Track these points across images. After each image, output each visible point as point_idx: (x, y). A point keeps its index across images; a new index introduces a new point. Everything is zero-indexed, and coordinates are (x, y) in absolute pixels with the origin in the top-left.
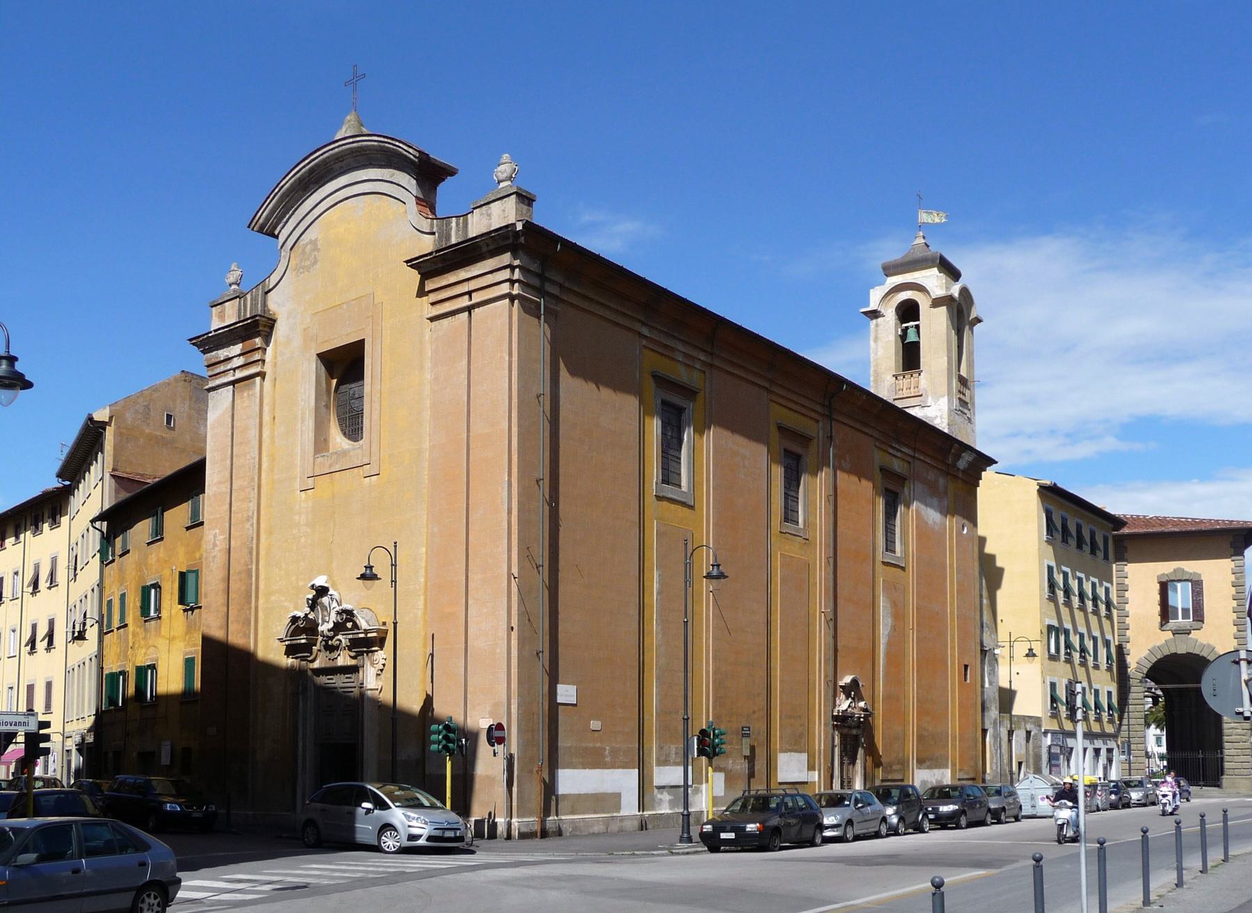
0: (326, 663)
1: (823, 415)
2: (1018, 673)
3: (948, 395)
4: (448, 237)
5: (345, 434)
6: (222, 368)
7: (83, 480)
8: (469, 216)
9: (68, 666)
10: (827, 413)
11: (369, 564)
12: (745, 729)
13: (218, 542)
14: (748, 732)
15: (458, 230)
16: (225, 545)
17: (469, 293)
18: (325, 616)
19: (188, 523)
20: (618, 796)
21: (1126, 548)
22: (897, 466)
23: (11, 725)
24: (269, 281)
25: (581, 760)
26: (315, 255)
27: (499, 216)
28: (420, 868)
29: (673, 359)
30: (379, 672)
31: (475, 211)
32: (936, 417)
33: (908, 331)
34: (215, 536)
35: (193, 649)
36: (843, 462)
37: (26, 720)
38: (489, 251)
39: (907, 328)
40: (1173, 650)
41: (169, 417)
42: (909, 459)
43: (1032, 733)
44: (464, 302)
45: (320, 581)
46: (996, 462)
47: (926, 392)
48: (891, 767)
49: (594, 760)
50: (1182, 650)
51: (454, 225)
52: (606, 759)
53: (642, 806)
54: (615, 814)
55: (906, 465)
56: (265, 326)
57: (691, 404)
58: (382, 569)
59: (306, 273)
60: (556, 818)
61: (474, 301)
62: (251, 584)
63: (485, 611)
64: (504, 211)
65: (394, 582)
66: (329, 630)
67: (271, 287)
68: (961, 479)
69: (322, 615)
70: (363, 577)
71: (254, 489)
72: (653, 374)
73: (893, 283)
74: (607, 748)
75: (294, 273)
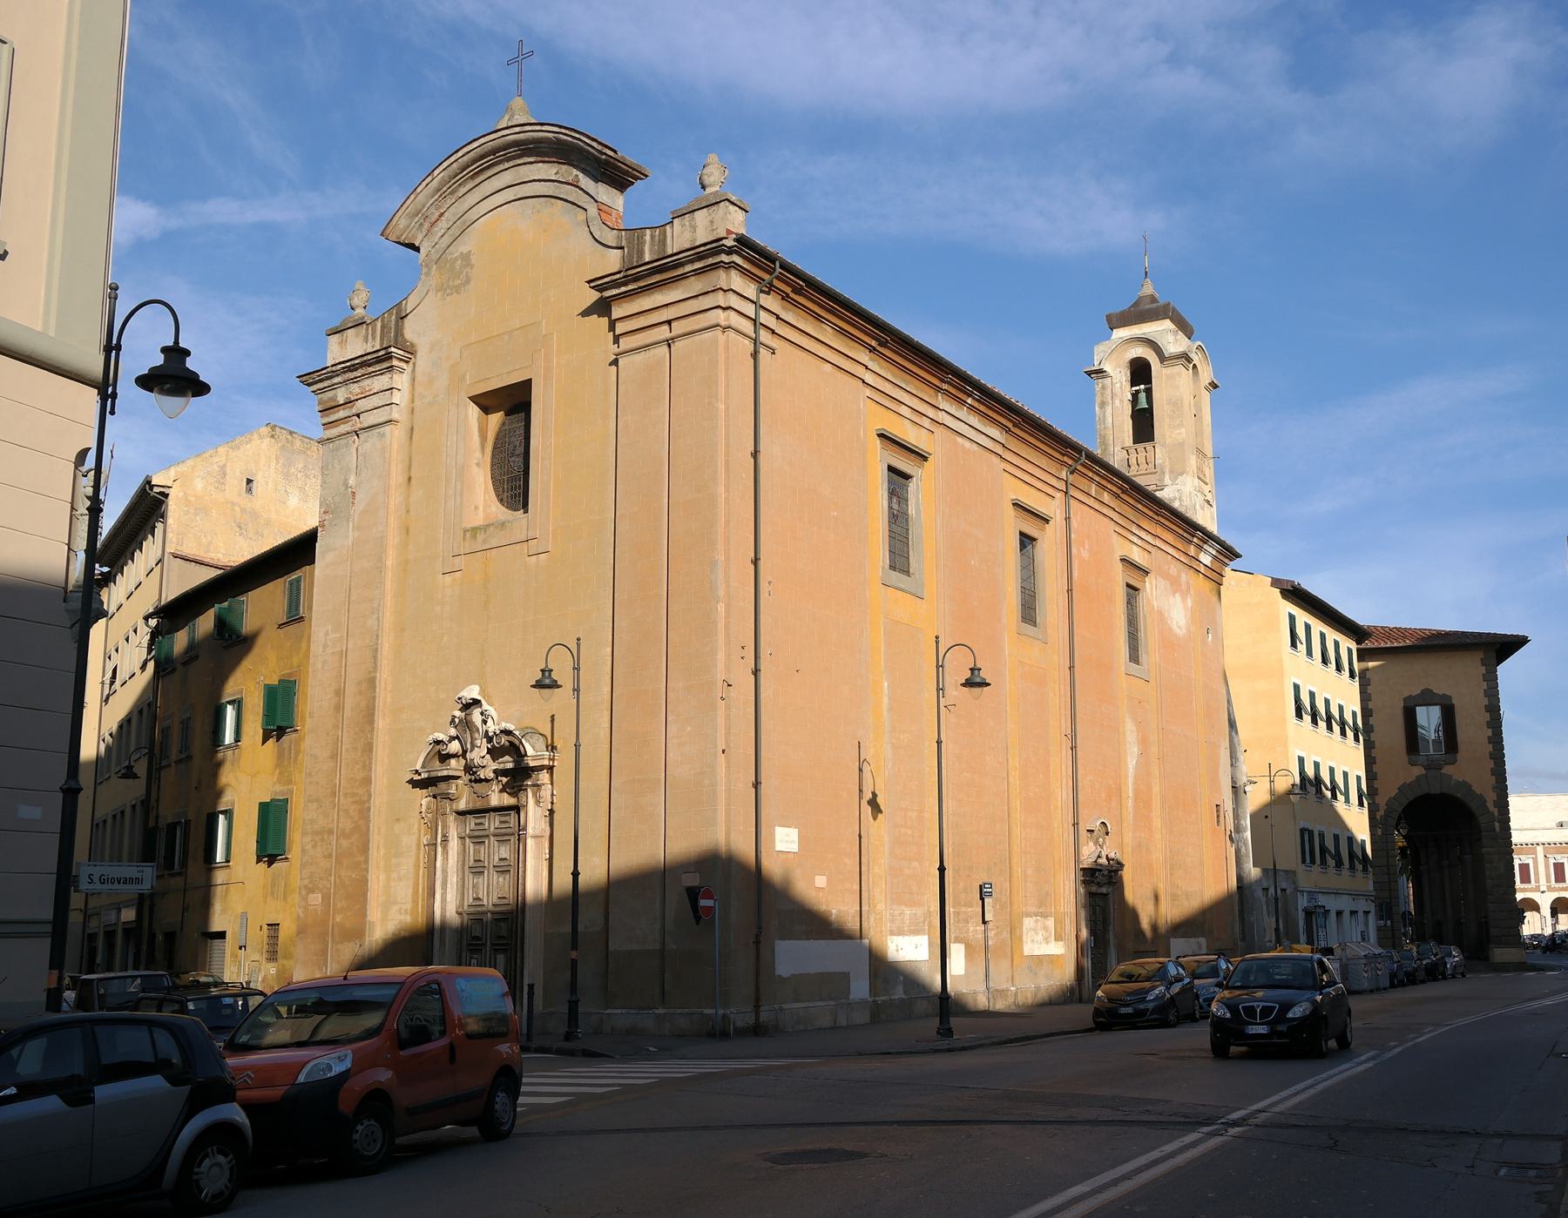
0: (475, 802)
4: (641, 253)
5: (501, 501)
6: (342, 414)
7: (130, 562)
8: (668, 227)
9: (96, 817)
11: (547, 666)
12: (986, 886)
13: (329, 643)
14: (990, 890)
15: (652, 244)
17: (669, 322)
19: (283, 619)
20: (845, 977)
23: (119, 883)
24: (406, 304)
27: (706, 228)
31: (675, 220)
32: (1176, 498)
34: (327, 634)
35: (286, 787)
37: (139, 875)
40: (1426, 791)
41: (249, 481)
44: (664, 333)
45: (473, 692)
51: (648, 238)
53: (873, 990)
58: (563, 674)
59: (455, 294)
60: (877, 999)
61: (674, 334)
64: (712, 222)
65: (577, 690)
67: (408, 312)
70: (539, 685)
73: (486, 488)
75: (439, 294)
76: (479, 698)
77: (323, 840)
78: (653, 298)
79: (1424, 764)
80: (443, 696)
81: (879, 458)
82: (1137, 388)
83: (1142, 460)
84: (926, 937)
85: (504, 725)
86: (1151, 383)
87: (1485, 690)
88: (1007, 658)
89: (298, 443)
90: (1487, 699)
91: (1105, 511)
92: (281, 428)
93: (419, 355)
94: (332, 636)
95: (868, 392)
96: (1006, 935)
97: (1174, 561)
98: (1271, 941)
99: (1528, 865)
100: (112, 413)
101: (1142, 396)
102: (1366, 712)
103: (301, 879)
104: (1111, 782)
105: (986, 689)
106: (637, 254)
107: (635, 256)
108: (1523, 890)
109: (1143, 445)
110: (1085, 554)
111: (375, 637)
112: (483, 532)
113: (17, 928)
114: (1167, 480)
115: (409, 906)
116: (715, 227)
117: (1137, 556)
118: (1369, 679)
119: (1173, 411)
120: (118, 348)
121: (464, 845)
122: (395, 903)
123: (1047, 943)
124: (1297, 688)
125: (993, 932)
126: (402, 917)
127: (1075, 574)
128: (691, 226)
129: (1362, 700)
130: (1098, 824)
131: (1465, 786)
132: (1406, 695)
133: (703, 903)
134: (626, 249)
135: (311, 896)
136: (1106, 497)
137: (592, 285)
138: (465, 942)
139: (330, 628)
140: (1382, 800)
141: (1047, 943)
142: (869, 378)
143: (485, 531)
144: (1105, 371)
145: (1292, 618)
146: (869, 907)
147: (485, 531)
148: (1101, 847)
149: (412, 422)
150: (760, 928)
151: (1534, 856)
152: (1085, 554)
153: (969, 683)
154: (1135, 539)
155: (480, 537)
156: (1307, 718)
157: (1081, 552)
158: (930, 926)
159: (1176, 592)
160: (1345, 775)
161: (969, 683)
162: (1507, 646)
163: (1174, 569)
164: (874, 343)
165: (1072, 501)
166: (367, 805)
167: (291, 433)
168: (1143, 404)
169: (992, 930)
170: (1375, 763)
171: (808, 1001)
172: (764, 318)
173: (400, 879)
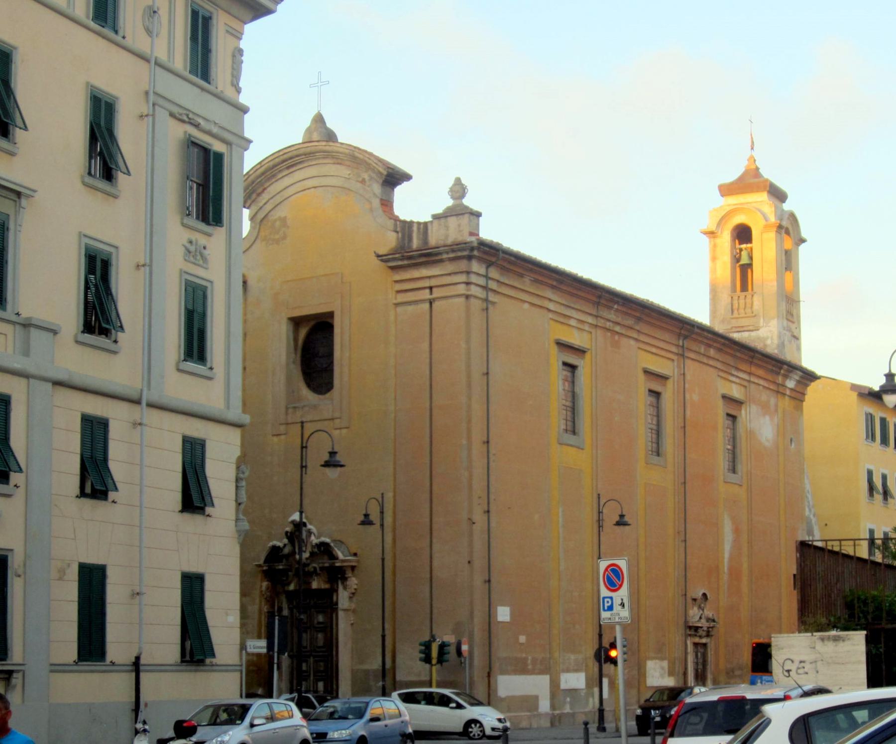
1: (677, 354)
2: (826, 525)
17: (431, 288)
20: (536, 698)
22: (736, 392)
29: (569, 325)
30: (351, 595)
42: (746, 383)
44: (426, 294)
48: (733, 672)
49: (521, 668)
53: (553, 707)
55: (743, 389)
57: (582, 362)
58: (375, 516)
70: (363, 523)
81: (556, 358)
85: (323, 539)
91: (711, 362)
95: (551, 315)
100: (306, 473)
101: (744, 254)
105: (627, 527)
110: (695, 397)
113: (163, 668)
120: (306, 447)
124: (870, 473)
127: (688, 413)
130: (700, 594)
136: (712, 352)
137: (380, 258)
142: (551, 306)
148: (703, 610)
150: (490, 668)
152: (695, 397)
153: (618, 524)
156: (879, 497)
157: (693, 397)
158: (587, 666)
161: (618, 524)
163: (765, 396)
164: (555, 283)
165: (688, 362)
168: (745, 260)
172: (493, 285)
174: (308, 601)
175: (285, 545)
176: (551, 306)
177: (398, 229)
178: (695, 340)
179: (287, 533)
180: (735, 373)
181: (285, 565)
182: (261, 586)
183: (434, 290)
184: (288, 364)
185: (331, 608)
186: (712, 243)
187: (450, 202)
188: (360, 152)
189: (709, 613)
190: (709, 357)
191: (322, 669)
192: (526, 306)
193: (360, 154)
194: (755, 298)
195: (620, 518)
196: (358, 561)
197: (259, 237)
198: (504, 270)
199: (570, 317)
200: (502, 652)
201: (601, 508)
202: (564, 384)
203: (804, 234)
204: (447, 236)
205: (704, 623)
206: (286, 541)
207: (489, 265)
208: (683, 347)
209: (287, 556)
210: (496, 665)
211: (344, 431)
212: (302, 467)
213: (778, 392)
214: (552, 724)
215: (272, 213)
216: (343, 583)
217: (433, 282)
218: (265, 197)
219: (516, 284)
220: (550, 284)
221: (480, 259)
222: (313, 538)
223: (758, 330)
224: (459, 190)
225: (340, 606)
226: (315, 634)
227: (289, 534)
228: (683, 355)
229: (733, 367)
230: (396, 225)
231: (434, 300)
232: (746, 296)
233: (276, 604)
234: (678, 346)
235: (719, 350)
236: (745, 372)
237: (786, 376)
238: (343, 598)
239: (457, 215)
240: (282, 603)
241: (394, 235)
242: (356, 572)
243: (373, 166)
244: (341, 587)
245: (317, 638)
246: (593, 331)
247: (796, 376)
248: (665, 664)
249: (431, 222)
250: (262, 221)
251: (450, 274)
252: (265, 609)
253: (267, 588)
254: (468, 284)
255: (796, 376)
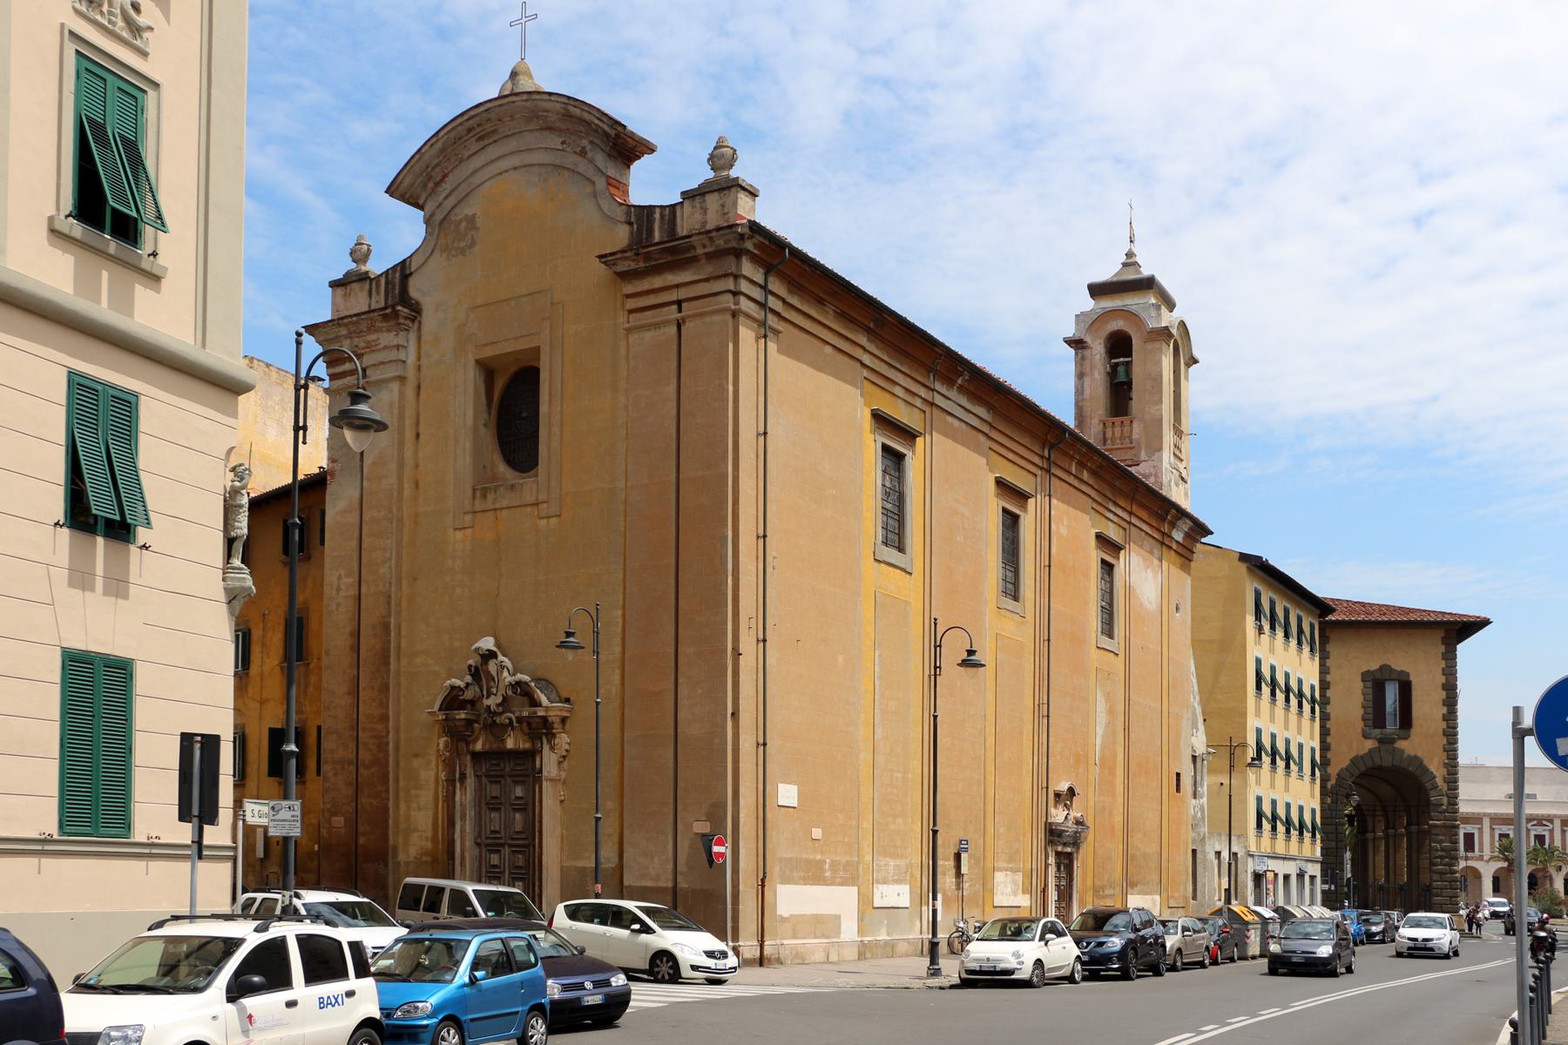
1: (1041, 468)
3: (1072, 433)
4: (650, 231)
10: (1045, 466)
13: (343, 587)
16: (353, 592)
17: (679, 303)
18: (492, 687)
20: (837, 919)
21: (1328, 637)
24: (410, 262)
25: (802, 874)
26: (472, 236)
27: (717, 212)
28: (659, 1002)
30: (561, 759)
33: (1118, 368)
34: (339, 578)
36: (1060, 526)
38: (706, 254)
39: (1117, 365)
42: (1126, 525)
43: (1239, 856)
45: (488, 643)
46: (1212, 533)
47: (1139, 444)
49: (814, 875)
50: (1387, 761)
52: (827, 874)
54: (834, 940)
55: (1121, 531)
56: (406, 318)
62: (389, 642)
63: (700, 691)
64: (723, 206)
66: (498, 705)
68: (1175, 551)
69: (487, 685)
71: (392, 522)
72: (874, 412)
74: (828, 860)
75: (445, 255)
76: (495, 649)
77: (343, 769)
78: (663, 277)
79: (1379, 737)
80: (456, 644)
82: (1117, 361)
83: (1118, 434)
84: (908, 886)
85: (520, 676)
86: (1130, 355)
87: (1443, 669)
88: (988, 632)
89: (274, 374)
90: (1444, 662)
91: (1084, 488)
92: (259, 360)
93: (424, 313)
94: (345, 580)
95: (865, 373)
96: (978, 887)
97: (1147, 537)
98: (1220, 900)
99: (1473, 834)
100: (304, 443)
101: (1121, 369)
102: (1324, 685)
103: (324, 803)
104: (1079, 749)
106: (647, 230)
107: (644, 233)
108: (1467, 859)
109: (1121, 419)
110: (1063, 531)
111: (388, 585)
112: (493, 493)
114: (1143, 456)
115: (430, 834)
116: (726, 211)
117: (1114, 533)
118: (1329, 652)
119: (1153, 387)
121: (480, 782)
122: (416, 830)
123: (1015, 896)
125: (968, 884)
126: (423, 843)
128: (701, 208)
129: (1321, 673)
130: (1066, 788)
131: (1417, 760)
132: (1365, 669)
133: (716, 849)
134: (635, 226)
135: (334, 819)
136: (1085, 475)
137: (603, 260)
138: (484, 870)
139: (342, 572)
140: (1333, 770)
141: (1015, 896)
142: (866, 359)
143: (495, 492)
144: (1085, 342)
145: (1258, 595)
146: (859, 857)
147: (495, 492)
149: (419, 379)
151: (1479, 826)
152: (1063, 531)
153: (965, 663)
154: (1111, 516)
155: (490, 497)
158: (912, 876)
159: (1148, 568)
160: (1301, 746)
161: (965, 663)
162: (1467, 627)
165: (1055, 481)
166: (385, 740)
167: (268, 365)
168: (1122, 377)
169: (966, 882)
170: (1329, 735)
171: (805, 938)
172: (773, 302)
173: (419, 809)
174: (502, 765)
175: (468, 685)
176: (866, 359)
177: (633, 219)
178: (1065, 454)
179: (470, 666)
180: (1113, 508)
181: (467, 713)
182: (438, 744)
183: (684, 305)
184: (475, 427)
185: (533, 777)
186: (1080, 355)
187: (710, 174)
188: (576, 104)
189: (1076, 813)
190: (1081, 480)
191: (521, 864)
192: (828, 349)
193: (575, 107)
194: (1135, 425)
195: (968, 655)
196: (571, 711)
197: (438, 247)
198: (794, 285)
199: (895, 383)
200: (782, 847)
201: (938, 639)
202: (884, 479)
203: (1196, 353)
204: (704, 223)
205: (1071, 827)
206: (469, 679)
207: (769, 270)
208: (1049, 459)
209: (472, 702)
210: (774, 870)
211: (554, 521)
212: (297, 428)
213: (1162, 543)
214: (861, 956)
215: (456, 210)
216: (549, 742)
217: (683, 294)
218: (447, 186)
219: (813, 313)
220: (866, 326)
221: (755, 259)
222: (505, 673)
223: (1138, 465)
224: (721, 158)
225: (545, 773)
226: (512, 813)
227: (473, 669)
228: (1048, 471)
229: (1110, 500)
230: (628, 214)
231: (684, 319)
232: (1122, 422)
233: (458, 768)
234: (1042, 457)
235: (1093, 473)
236: (1124, 509)
237: (1173, 525)
238: (549, 762)
239: (720, 190)
240: (465, 768)
241: (626, 228)
242: (567, 726)
243: (596, 125)
244: (546, 748)
245: (514, 818)
246: (927, 409)
247: (1185, 525)
248: (1019, 877)
249: (682, 203)
250: (440, 224)
251: (707, 280)
252: (443, 776)
253: (446, 746)
254: (736, 294)
255: (1185, 525)
